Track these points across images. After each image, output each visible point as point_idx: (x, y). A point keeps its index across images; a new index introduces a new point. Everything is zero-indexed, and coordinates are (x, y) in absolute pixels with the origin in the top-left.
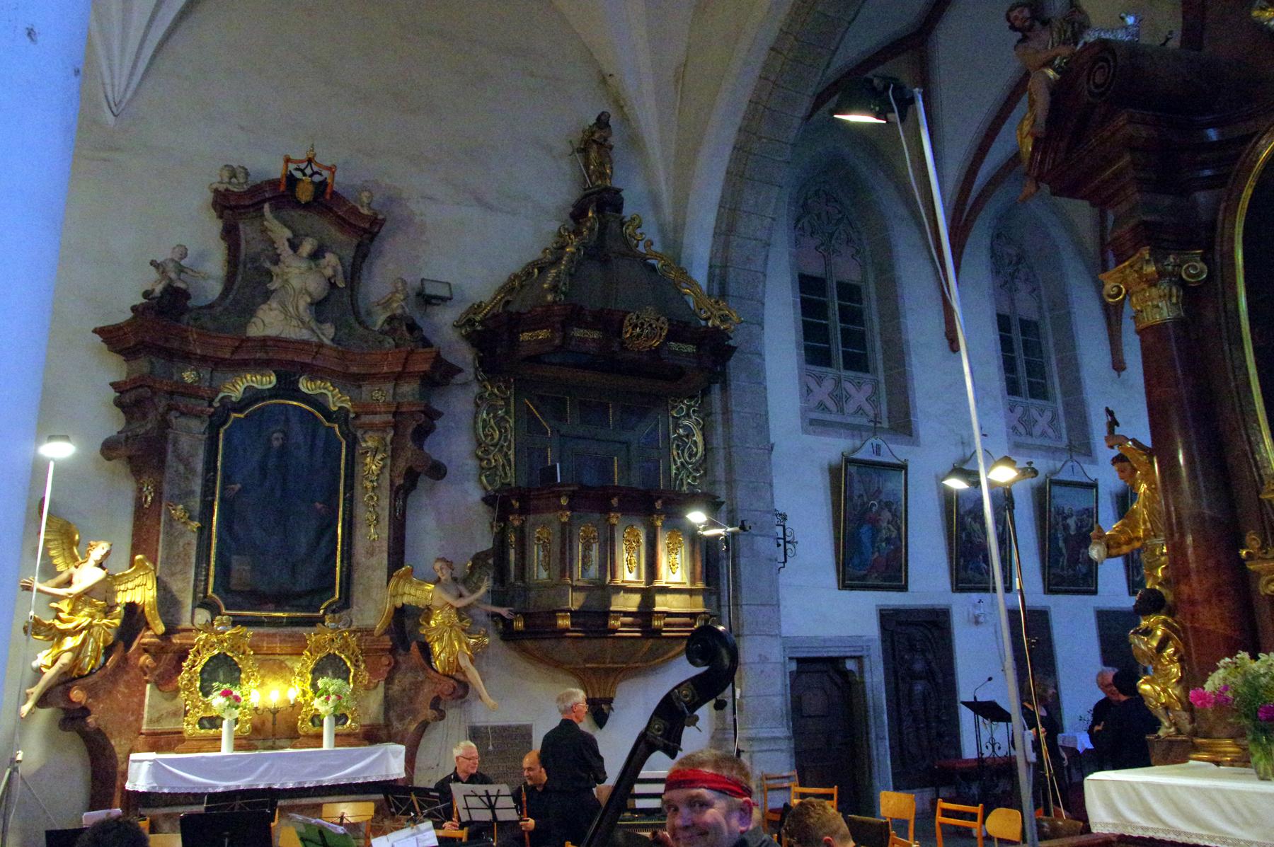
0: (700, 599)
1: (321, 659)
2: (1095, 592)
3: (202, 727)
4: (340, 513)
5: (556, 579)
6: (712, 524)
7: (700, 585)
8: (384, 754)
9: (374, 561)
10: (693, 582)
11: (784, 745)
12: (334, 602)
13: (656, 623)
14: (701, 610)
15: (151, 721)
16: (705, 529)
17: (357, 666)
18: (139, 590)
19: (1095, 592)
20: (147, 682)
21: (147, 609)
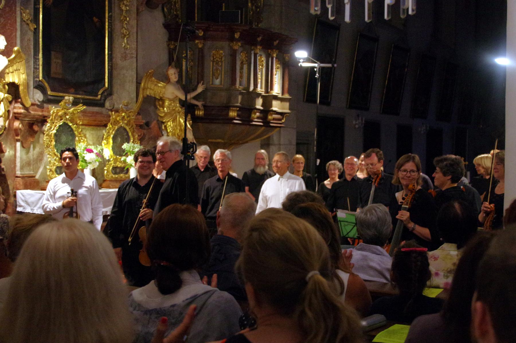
0: (287, 104)
1: (60, 126)
2: (367, 109)
3: (115, 173)
4: (107, 27)
5: (53, 75)
6: (307, 60)
7: (287, 96)
8: (263, 194)
9: (126, 63)
10: (283, 93)
11: (300, 190)
12: (105, 90)
13: (270, 117)
14: (287, 111)
15: (22, 168)
16: (303, 62)
17: (134, 136)
18: (15, 74)
19: (367, 109)
20: (18, 140)
21: (21, 88)
